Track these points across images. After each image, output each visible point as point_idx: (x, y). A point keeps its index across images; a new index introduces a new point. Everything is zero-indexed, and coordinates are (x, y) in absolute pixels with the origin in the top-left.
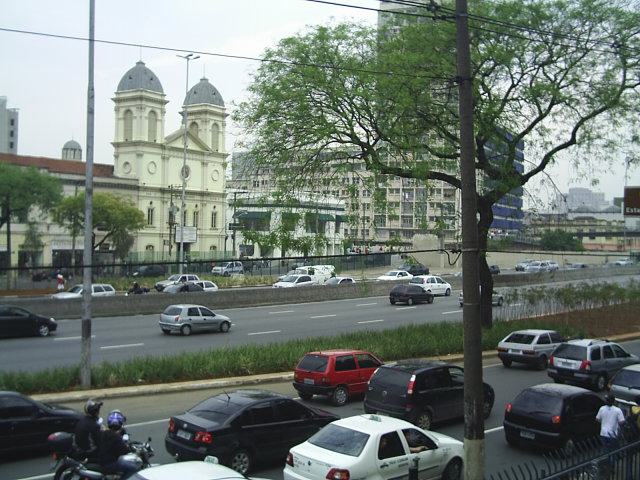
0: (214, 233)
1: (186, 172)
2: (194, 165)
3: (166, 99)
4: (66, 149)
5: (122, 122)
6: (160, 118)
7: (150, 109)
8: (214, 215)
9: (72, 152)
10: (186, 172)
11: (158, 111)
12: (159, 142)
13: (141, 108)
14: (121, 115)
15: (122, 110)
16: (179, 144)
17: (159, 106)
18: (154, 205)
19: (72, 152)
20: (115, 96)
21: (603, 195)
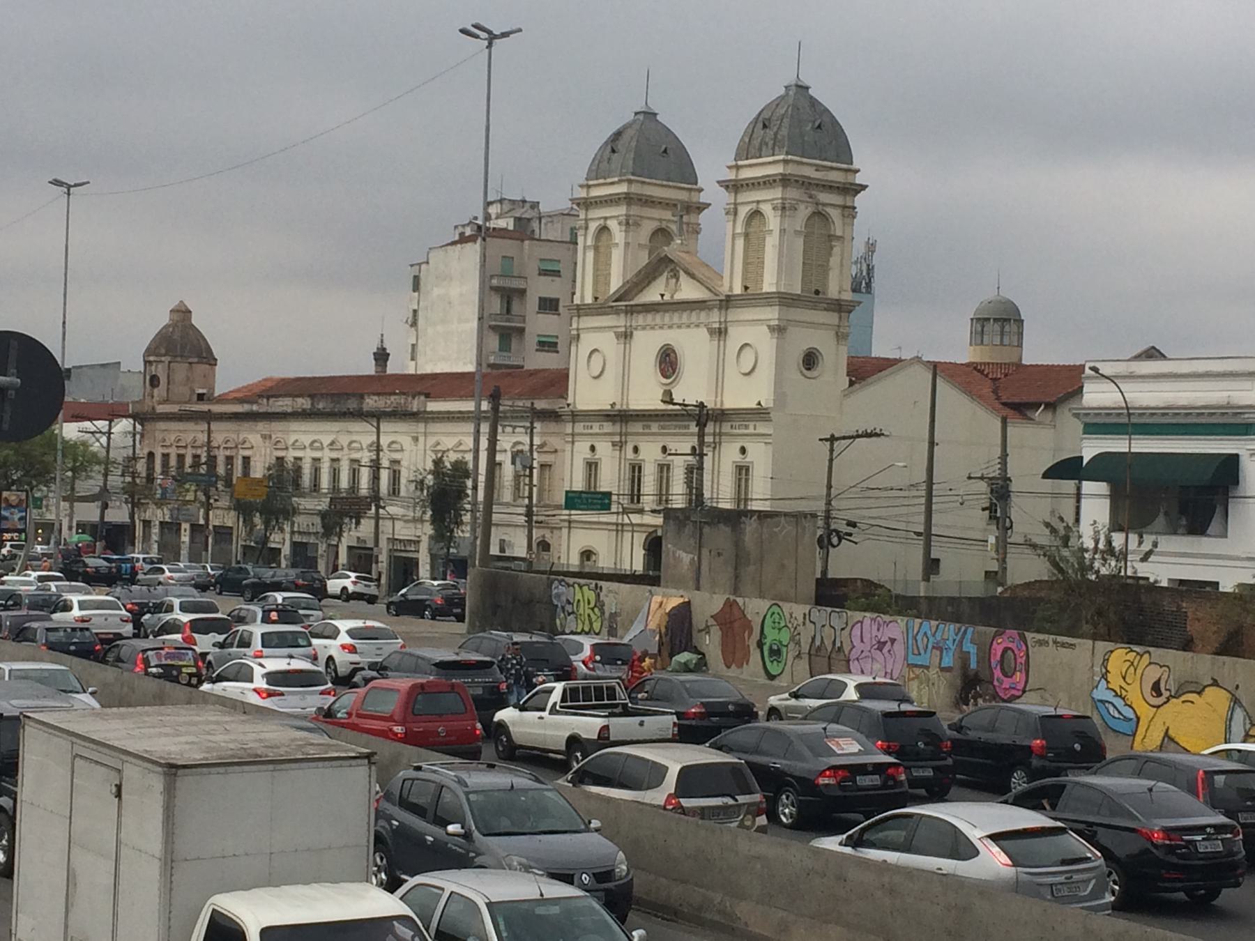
1: (668, 362)
2: (692, 342)
4: (981, 322)
6: (839, 233)
7: (654, 225)
9: (997, 327)
10: (668, 362)
11: (834, 214)
12: (833, 291)
15: (743, 211)
16: (652, 295)
18: (750, 457)
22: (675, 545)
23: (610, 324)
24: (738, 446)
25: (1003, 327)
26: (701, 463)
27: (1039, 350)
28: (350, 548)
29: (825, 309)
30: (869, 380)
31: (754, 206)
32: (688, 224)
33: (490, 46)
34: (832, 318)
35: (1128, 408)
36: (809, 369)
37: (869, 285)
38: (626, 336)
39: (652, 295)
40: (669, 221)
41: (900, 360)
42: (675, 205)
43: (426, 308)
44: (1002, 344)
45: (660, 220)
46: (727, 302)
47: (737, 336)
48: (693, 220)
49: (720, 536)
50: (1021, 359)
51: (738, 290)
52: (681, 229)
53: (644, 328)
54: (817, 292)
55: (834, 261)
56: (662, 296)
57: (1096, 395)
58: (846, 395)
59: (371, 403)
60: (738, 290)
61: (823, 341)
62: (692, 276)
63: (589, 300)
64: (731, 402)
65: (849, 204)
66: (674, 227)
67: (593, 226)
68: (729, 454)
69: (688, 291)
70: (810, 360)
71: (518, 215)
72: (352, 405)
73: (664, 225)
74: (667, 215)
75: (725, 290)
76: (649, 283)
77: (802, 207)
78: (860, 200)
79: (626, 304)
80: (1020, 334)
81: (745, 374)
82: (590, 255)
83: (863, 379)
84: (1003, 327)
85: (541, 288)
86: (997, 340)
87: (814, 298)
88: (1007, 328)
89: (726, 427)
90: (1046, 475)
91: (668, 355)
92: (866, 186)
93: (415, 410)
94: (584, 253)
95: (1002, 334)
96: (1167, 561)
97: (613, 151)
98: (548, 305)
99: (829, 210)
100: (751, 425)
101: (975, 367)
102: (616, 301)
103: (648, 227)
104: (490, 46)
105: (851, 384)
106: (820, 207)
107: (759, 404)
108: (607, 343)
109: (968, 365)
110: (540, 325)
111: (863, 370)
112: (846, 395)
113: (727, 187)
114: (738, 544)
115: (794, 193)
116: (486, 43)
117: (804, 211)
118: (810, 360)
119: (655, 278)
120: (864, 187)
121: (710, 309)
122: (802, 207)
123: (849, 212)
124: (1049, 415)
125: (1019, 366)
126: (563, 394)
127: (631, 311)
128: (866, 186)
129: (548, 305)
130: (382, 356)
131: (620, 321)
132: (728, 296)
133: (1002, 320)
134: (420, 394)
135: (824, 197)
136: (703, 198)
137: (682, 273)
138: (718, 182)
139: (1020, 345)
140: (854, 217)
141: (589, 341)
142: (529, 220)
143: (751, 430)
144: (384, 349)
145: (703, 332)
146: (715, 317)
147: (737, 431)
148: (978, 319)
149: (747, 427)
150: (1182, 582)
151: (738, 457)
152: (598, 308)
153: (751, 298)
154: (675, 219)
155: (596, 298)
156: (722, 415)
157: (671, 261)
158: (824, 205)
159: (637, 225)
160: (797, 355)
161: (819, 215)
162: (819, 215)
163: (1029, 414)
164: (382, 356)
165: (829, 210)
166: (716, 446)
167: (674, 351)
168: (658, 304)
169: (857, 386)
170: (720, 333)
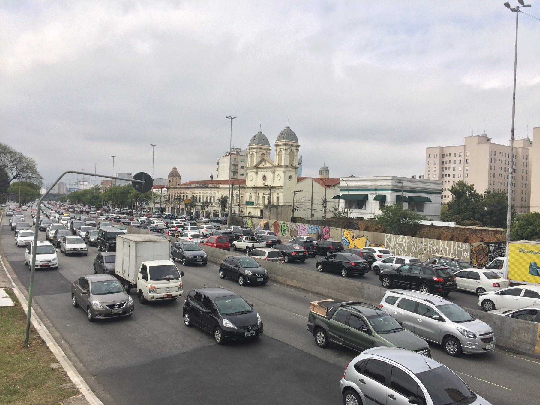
1: (264, 178)
2: (269, 174)
3: (299, 144)
4: (321, 171)
10: (264, 178)
11: (295, 151)
12: (294, 165)
15: (278, 150)
16: (261, 165)
34: (294, 170)
38: (257, 173)
39: (261, 165)
46: (275, 167)
49: (274, 210)
51: (277, 165)
55: (295, 159)
57: (342, 184)
59: (210, 185)
60: (277, 165)
61: (293, 174)
68: (276, 195)
69: (268, 165)
70: (290, 177)
72: (206, 186)
74: (264, 151)
78: (299, 148)
79: (257, 167)
87: (291, 166)
89: (275, 190)
96: (355, 214)
98: (243, 167)
108: (253, 174)
110: (241, 171)
111: (300, 179)
112: (297, 184)
115: (287, 147)
117: (289, 150)
118: (290, 177)
123: (297, 150)
125: (328, 179)
127: (258, 168)
129: (243, 167)
130: (212, 177)
131: (255, 170)
135: (293, 148)
141: (250, 174)
145: (271, 172)
146: (273, 170)
152: (251, 168)
153: (280, 166)
156: (274, 188)
161: (292, 151)
162: (292, 151)
164: (212, 177)
166: (273, 193)
170: (274, 172)
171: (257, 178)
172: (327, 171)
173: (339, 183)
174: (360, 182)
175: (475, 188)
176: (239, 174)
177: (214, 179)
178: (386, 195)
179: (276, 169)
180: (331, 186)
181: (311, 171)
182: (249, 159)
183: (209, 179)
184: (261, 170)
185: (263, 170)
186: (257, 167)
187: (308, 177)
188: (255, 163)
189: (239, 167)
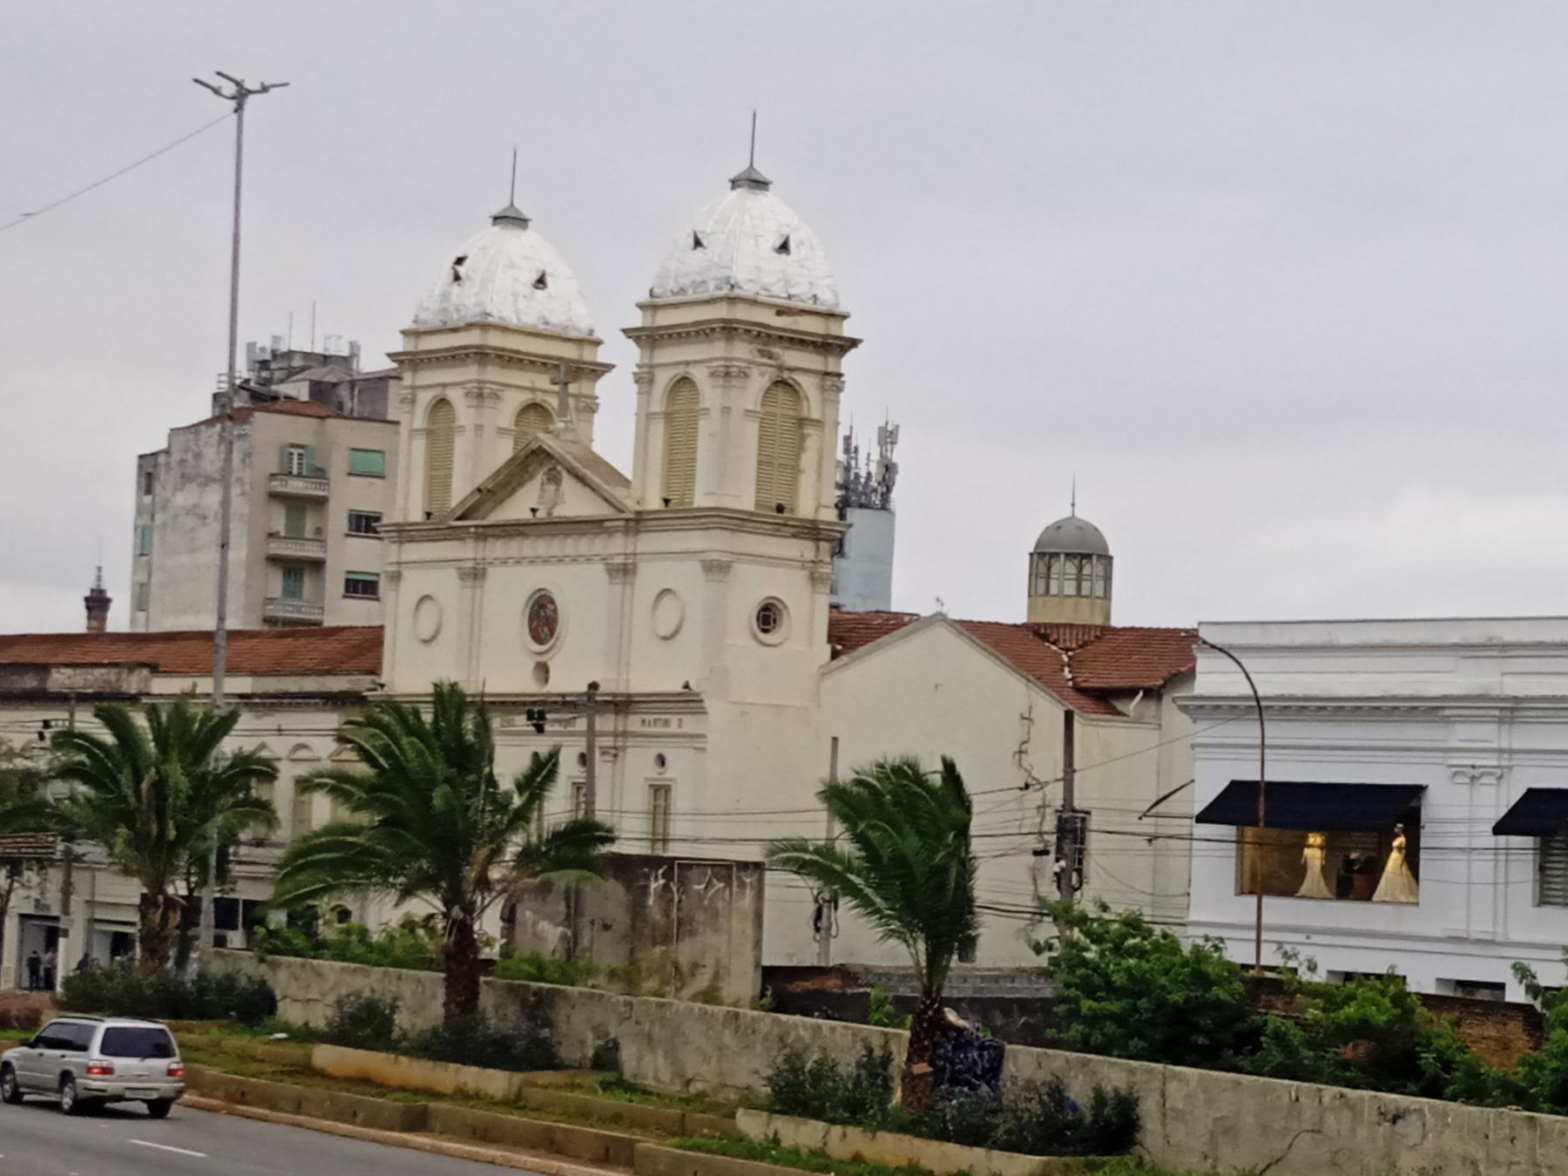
0: (42, 744)
1: (542, 618)
2: (578, 585)
3: (848, 330)
4: (1044, 557)
5: (658, 429)
6: (815, 415)
7: (523, 398)
8: (660, 791)
9: (1071, 568)
10: (542, 618)
11: (808, 384)
12: (805, 508)
13: (480, 395)
14: (657, 406)
15: (664, 378)
16: (517, 508)
17: (813, 361)
18: (671, 772)
19: (1071, 568)
20: (637, 320)
21: (87, 599)
22: (535, 912)
23: (450, 556)
24: (654, 752)
25: (1080, 569)
26: (591, 775)
27: (1134, 605)
28: (23, 917)
29: (794, 536)
30: (862, 649)
31: (681, 370)
32: (577, 397)
33: (239, 109)
34: (806, 549)
35: (1257, 699)
36: (765, 631)
37: (885, 497)
38: (475, 574)
39: (517, 508)
40: (545, 391)
41: (914, 617)
42: (556, 366)
43: (164, 525)
44: (1079, 593)
45: (533, 390)
46: (637, 523)
47: (651, 576)
48: (585, 391)
49: (607, 897)
50: (1107, 616)
51: (654, 503)
52: (563, 405)
53: (504, 562)
54: (780, 509)
55: (807, 460)
56: (534, 510)
57: (1213, 678)
58: (824, 673)
59: (60, 679)
60: (654, 503)
61: (791, 589)
62: (581, 479)
63: (417, 516)
64: (639, 682)
65: (831, 369)
66: (553, 402)
67: (424, 398)
68: (638, 764)
69: (575, 503)
70: (768, 617)
71: (314, 378)
72: (29, 682)
73: (539, 397)
74: (542, 381)
75: (631, 505)
76: (514, 490)
77: (755, 372)
78: (849, 364)
79: (471, 520)
80: (1108, 579)
81: (665, 638)
82: (420, 446)
83: (853, 647)
84: (1080, 569)
85: (348, 496)
86: (1070, 588)
87: (777, 518)
88: (1087, 571)
89: (634, 723)
90: (1499, 829)
91: (542, 607)
92: (860, 341)
93: (133, 691)
94: (410, 445)
95: (1079, 578)
96: (1321, 938)
97: (457, 278)
98: (364, 524)
99: (799, 377)
100: (674, 719)
101: (1038, 632)
102: (460, 518)
103: (514, 401)
104: (239, 109)
105: (835, 655)
106: (786, 375)
107: (686, 686)
108: (444, 584)
109: (1024, 625)
110: (352, 554)
111: (851, 634)
112: (824, 673)
113: (637, 340)
114: (637, 908)
115: (742, 351)
116: (233, 104)
117: (759, 381)
118: (768, 617)
119: (521, 484)
120: (854, 343)
121: (610, 532)
122: (755, 372)
123: (832, 381)
124: (1151, 706)
125: (1106, 631)
126: (375, 671)
127: (486, 534)
128: (860, 341)
129: (364, 524)
130: (97, 603)
131: (466, 550)
132: (638, 513)
133: (1071, 554)
134: (142, 665)
135: (792, 357)
136: (602, 355)
137: (564, 474)
138: (624, 331)
139: (1107, 596)
140: (840, 390)
141: (415, 583)
142: (335, 385)
143: (673, 729)
144: (102, 592)
145: (598, 569)
146: (617, 545)
147: (647, 730)
148: (1041, 555)
149: (666, 723)
150: (1348, 976)
151: (652, 771)
152: (436, 527)
153: (677, 513)
154: (556, 388)
155: (429, 515)
156: (623, 704)
157: (548, 455)
158: (791, 370)
159: (496, 396)
160: (746, 612)
161: (783, 385)
162: (783, 385)
163: (1120, 706)
164: (97, 603)
165: (799, 377)
166: (615, 753)
167: (552, 602)
168: (527, 524)
169: (844, 659)
170: (624, 571)
171: (474, 617)
172: (1092, 568)
173: (1192, 673)
174: (1314, 662)
175: (312, 1025)
176: (334, 582)
177: (119, 620)
178: (1417, 791)
179: (648, 542)
180: (1130, 693)
181: (956, 558)
182: (411, 455)
183: (74, 621)
184: (513, 547)
185: (540, 547)
186: (471, 520)
187: (926, 610)
188: (460, 491)
189: (337, 521)
